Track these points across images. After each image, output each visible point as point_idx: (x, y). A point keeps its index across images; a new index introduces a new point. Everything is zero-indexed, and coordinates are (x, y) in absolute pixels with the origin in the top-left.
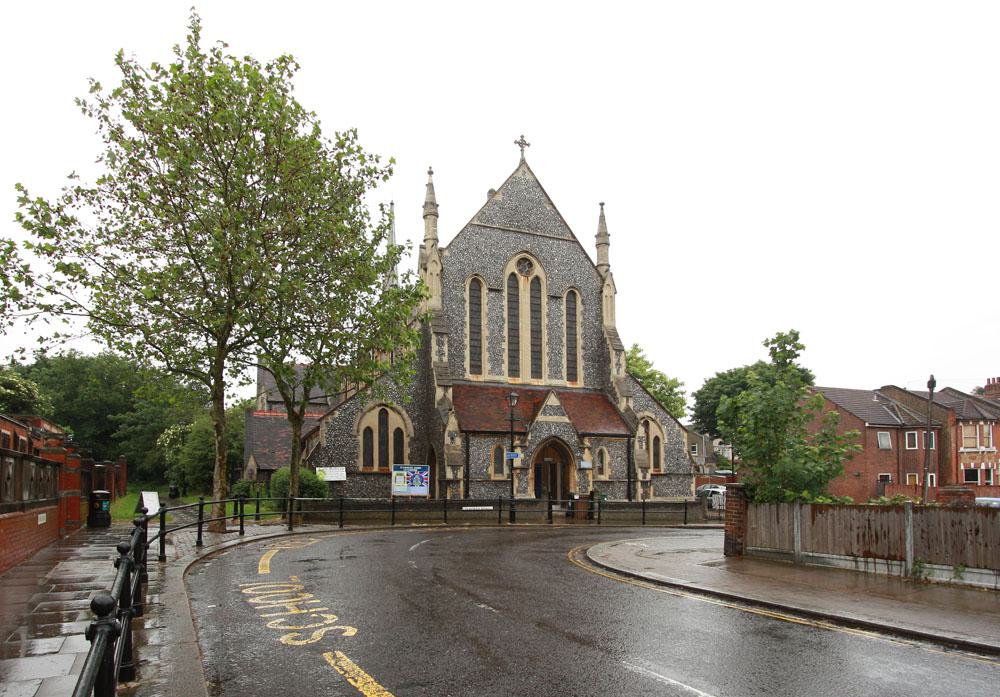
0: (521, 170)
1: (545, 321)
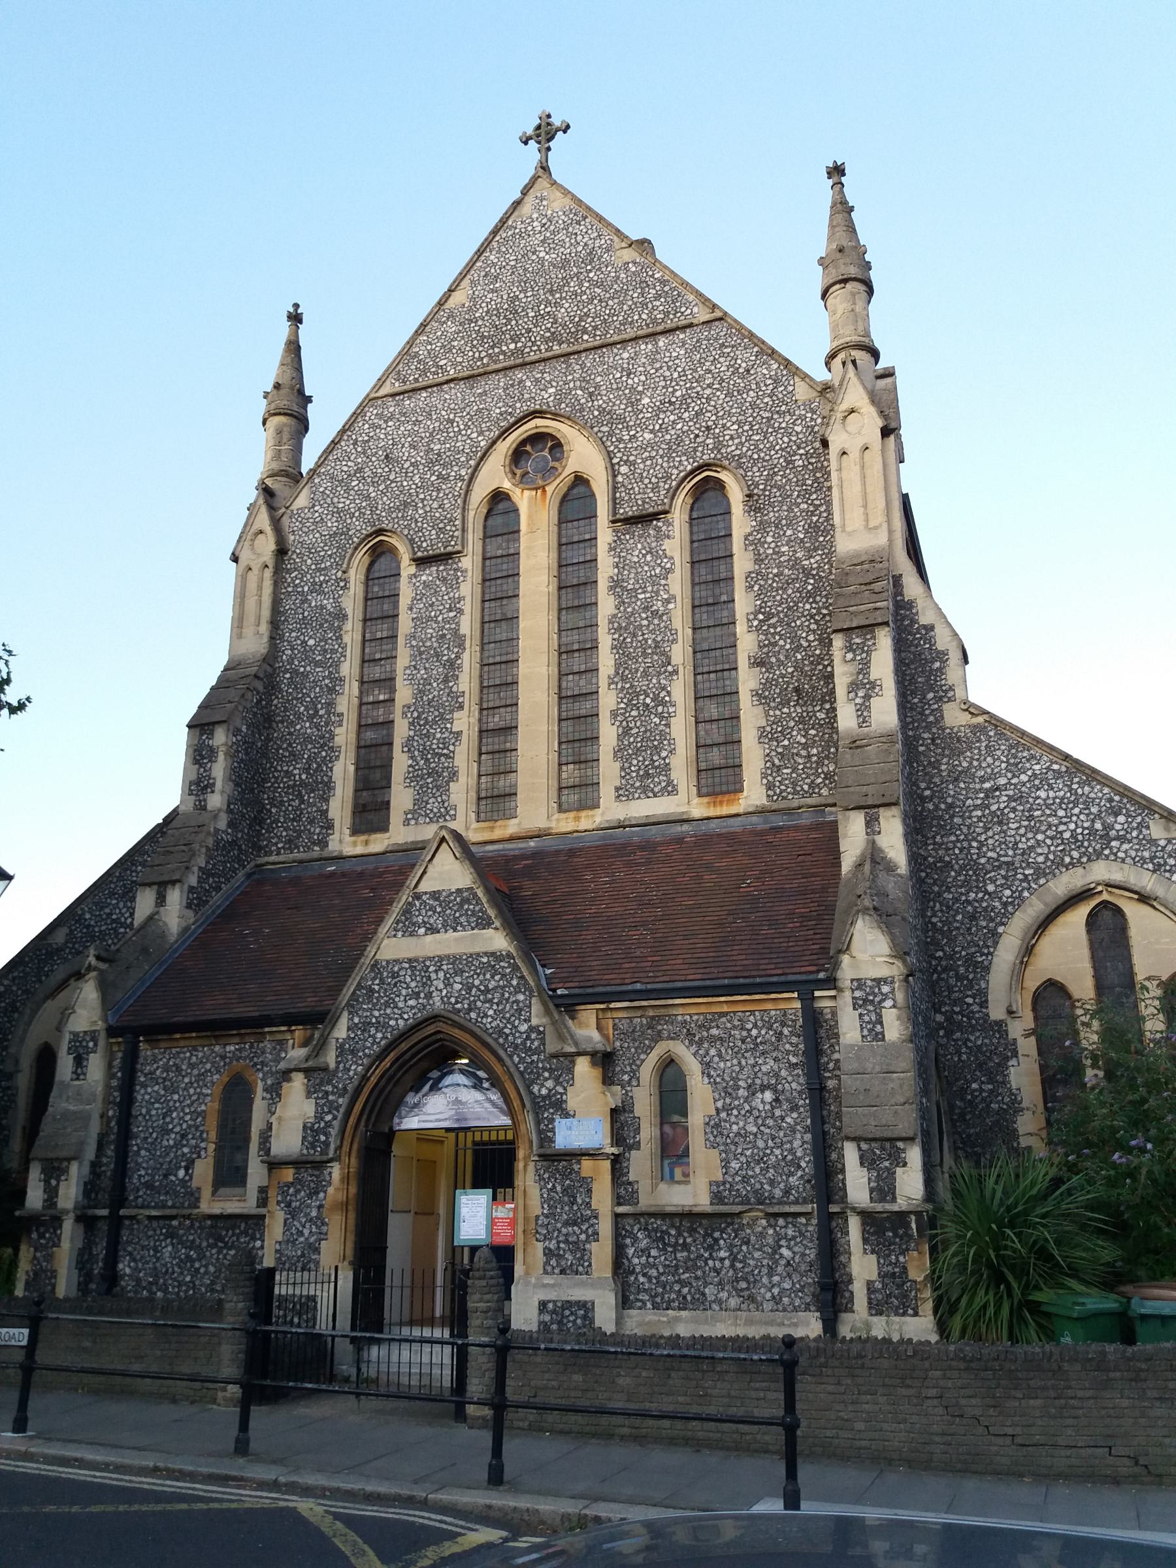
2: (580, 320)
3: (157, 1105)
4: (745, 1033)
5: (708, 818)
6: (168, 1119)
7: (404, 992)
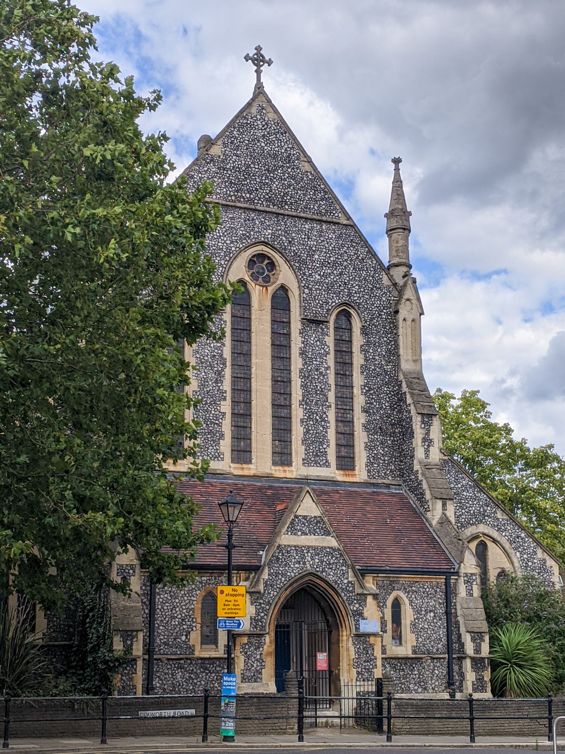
0: (255, 104)
1: (297, 363)
2: (284, 196)
3: (167, 604)
4: (424, 590)
5: (345, 482)
6: (174, 612)
7: (293, 560)
